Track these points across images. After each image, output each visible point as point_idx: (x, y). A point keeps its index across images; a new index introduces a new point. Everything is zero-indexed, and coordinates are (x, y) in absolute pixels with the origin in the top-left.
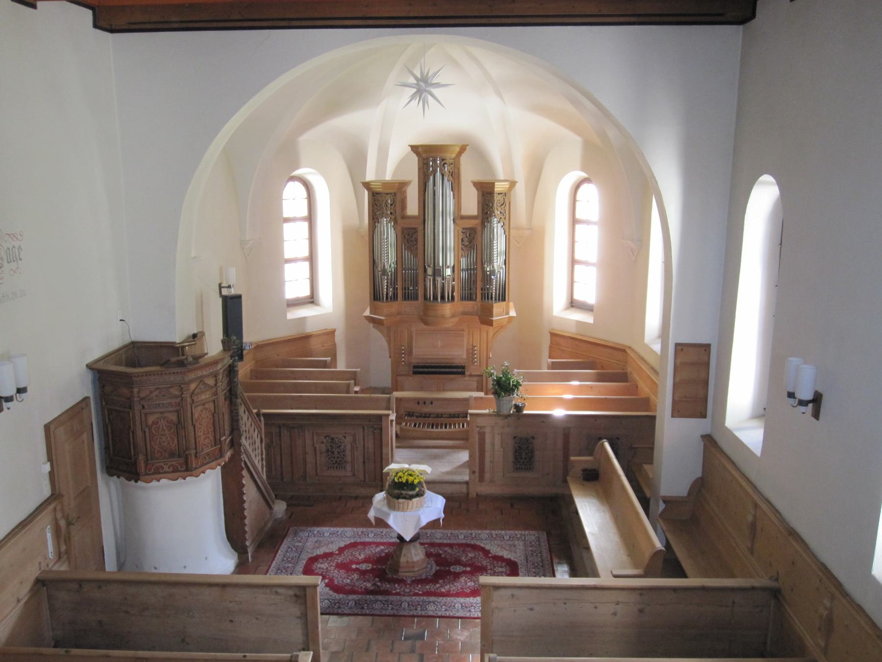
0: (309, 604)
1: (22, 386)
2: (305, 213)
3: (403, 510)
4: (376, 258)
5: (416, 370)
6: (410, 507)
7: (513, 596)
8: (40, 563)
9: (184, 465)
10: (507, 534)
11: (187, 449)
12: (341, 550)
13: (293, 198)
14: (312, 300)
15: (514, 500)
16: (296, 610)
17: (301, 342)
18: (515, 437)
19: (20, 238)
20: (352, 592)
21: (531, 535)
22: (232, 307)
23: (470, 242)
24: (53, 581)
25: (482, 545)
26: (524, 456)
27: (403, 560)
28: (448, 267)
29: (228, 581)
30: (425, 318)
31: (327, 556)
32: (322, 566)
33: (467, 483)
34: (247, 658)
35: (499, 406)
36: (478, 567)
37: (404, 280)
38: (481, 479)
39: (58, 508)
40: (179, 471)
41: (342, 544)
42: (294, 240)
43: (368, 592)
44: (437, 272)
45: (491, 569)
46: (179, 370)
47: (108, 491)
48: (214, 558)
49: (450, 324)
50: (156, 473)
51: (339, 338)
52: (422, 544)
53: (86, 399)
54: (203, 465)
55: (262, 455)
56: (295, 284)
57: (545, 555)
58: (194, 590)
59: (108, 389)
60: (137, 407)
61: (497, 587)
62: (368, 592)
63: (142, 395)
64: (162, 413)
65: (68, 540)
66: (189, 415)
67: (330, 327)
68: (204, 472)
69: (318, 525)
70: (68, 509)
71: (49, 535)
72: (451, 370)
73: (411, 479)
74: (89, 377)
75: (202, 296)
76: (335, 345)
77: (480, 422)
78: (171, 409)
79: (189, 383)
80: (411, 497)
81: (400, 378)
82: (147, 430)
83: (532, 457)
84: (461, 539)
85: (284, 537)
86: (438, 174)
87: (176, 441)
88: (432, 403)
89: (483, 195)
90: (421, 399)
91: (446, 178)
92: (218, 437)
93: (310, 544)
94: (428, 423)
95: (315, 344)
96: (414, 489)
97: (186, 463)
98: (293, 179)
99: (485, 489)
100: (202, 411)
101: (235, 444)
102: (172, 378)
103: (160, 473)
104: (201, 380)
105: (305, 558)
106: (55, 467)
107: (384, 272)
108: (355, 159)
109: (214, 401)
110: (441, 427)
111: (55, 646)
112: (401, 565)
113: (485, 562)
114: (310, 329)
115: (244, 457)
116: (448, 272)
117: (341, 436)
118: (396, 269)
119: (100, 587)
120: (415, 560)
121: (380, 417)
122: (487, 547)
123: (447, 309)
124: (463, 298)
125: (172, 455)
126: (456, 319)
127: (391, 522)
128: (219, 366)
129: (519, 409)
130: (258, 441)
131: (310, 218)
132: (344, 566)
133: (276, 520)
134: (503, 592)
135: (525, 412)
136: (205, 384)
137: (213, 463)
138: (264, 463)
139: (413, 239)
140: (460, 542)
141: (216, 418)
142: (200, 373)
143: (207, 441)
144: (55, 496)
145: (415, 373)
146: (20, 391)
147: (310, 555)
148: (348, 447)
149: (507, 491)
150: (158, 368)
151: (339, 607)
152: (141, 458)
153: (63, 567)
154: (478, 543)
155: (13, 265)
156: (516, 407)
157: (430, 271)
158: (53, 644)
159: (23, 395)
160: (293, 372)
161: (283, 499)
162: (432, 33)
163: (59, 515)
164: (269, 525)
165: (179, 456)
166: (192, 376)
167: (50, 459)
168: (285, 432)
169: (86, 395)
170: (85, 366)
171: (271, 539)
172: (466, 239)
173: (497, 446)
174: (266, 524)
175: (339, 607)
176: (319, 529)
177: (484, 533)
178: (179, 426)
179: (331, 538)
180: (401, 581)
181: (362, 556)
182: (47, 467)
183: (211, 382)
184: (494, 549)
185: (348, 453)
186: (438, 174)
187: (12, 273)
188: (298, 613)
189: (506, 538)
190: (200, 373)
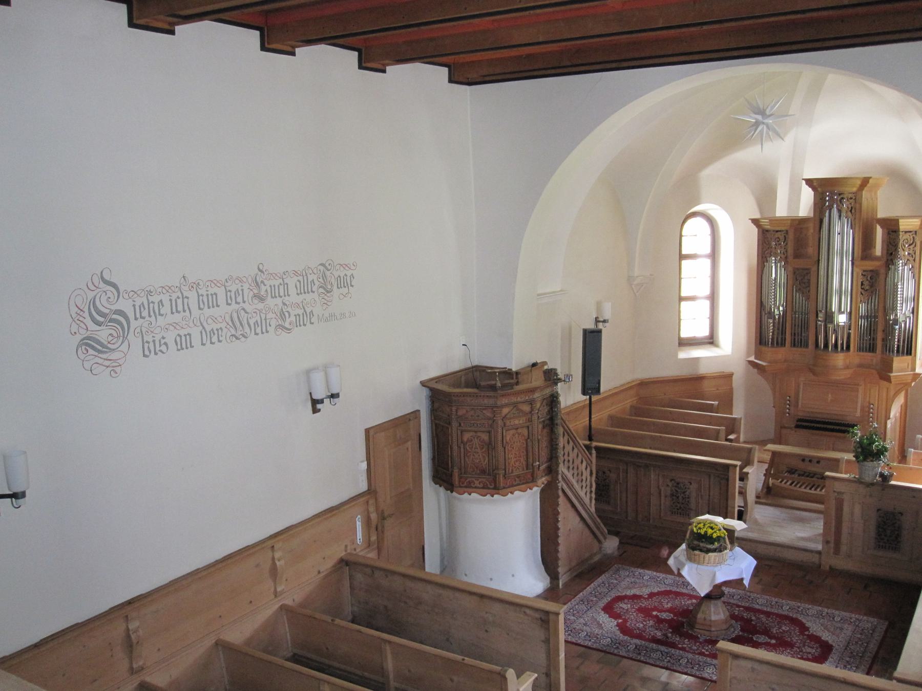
0: (551, 630)
1: (335, 392)
2: (708, 250)
3: (699, 563)
4: (763, 300)
5: (800, 423)
6: (706, 561)
7: (753, 670)
8: (346, 546)
9: (494, 482)
10: (839, 614)
11: (497, 468)
12: (651, 595)
13: (695, 236)
14: (711, 340)
15: (868, 582)
16: (539, 634)
17: (692, 384)
18: (878, 510)
19: (353, 267)
20: (639, 637)
21: (867, 622)
22: (592, 340)
23: (871, 286)
24: (355, 563)
25: (804, 621)
26: (888, 532)
27: (700, 616)
28: (843, 313)
29: (530, 603)
30: (816, 368)
31: (635, 597)
32: (625, 606)
33: (819, 553)
34: (465, 662)
35: (861, 474)
36: (787, 642)
37: (794, 326)
38: (837, 550)
39: (371, 502)
40: (489, 488)
41: (655, 590)
42: (694, 278)
43: (655, 640)
44: (829, 317)
45: (799, 648)
46: (492, 394)
47: (432, 496)
48: (526, 580)
49: (842, 375)
50: (469, 487)
51: (738, 382)
52: (724, 602)
53: (416, 413)
54: (513, 486)
55: (591, 487)
56: (693, 322)
57: (871, 646)
58: (457, 594)
59: (436, 405)
60: (455, 424)
61: (736, 656)
62: (655, 640)
63: (460, 413)
64: (476, 432)
65: (379, 530)
66: (500, 438)
67: (728, 370)
68: (512, 493)
69: (643, 568)
70: (387, 504)
71: (359, 525)
72: (835, 428)
73: (710, 531)
74: (424, 393)
75: (570, 328)
76: (731, 390)
77: (838, 487)
78: (483, 429)
79: (503, 406)
80: (708, 551)
81: (784, 431)
82: (462, 446)
83: (898, 536)
84: (785, 610)
85: (604, 572)
86: (835, 210)
87: (486, 461)
88: (818, 462)
89: (889, 234)
90: (808, 456)
91: (844, 214)
92: (531, 460)
93: (624, 584)
94: (792, 483)
95: (707, 387)
96: (713, 543)
97: (495, 481)
98: (694, 214)
99: (840, 563)
100: (513, 435)
101: (551, 470)
102: (486, 401)
103: (471, 487)
104: (515, 405)
105: (614, 594)
106: (372, 464)
107: (771, 314)
108: (765, 193)
109: (528, 427)
110: (816, 490)
111: (353, 621)
112: (698, 621)
113: (796, 638)
114: (703, 370)
115: (561, 484)
116: (842, 319)
117: (686, 482)
118: (785, 312)
119: (387, 576)
120: (713, 618)
121: (727, 466)
122: (808, 624)
123: (840, 359)
124: (860, 349)
125: (483, 472)
126: (851, 371)
127: (684, 572)
128: (537, 395)
129: (885, 478)
130: (586, 474)
131: (714, 256)
132: (646, 612)
133: (605, 555)
134: (743, 663)
135: (893, 482)
136: (518, 409)
137: (523, 486)
138: (593, 496)
139: (806, 281)
140: (784, 613)
141: (530, 444)
142: (514, 399)
143: (517, 464)
144: (371, 492)
145: (797, 427)
146: (333, 396)
147: (619, 594)
148: (694, 494)
149: (867, 570)
150: (475, 390)
151: (617, 648)
152: (456, 471)
153: (372, 555)
154: (801, 618)
155: (345, 290)
156: (882, 475)
157: (821, 316)
158: (350, 618)
159: (336, 400)
160: (671, 412)
161: (617, 534)
162: (749, 64)
163: (372, 509)
164: (596, 558)
165: (489, 474)
166: (505, 401)
167: (368, 459)
168: (631, 470)
169: (418, 408)
170: (418, 382)
171: (588, 571)
172: (866, 283)
173: (858, 517)
174: (591, 557)
175: (617, 648)
176: (642, 571)
177: (814, 609)
178: (490, 446)
179: (643, 582)
180: (694, 638)
181: (669, 605)
182: (364, 465)
183: (526, 408)
184: (815, 628)
185: (693, 500)
186: (835, 210)
187: (342, 297)
188: (543, 638)
189: (837, 619)
190: (514, 399)
